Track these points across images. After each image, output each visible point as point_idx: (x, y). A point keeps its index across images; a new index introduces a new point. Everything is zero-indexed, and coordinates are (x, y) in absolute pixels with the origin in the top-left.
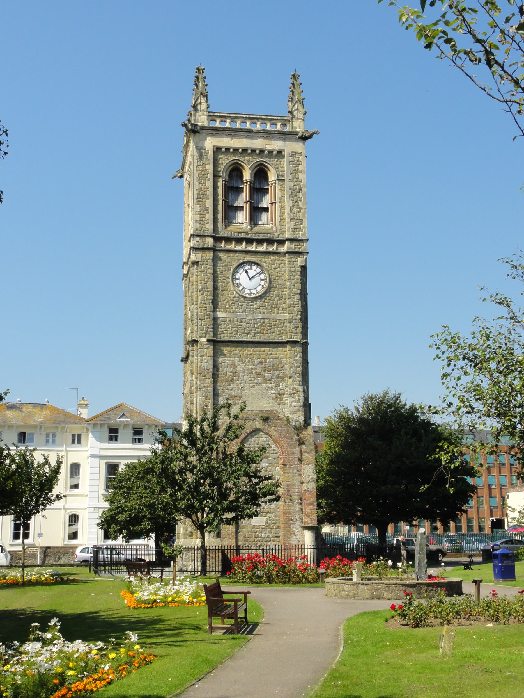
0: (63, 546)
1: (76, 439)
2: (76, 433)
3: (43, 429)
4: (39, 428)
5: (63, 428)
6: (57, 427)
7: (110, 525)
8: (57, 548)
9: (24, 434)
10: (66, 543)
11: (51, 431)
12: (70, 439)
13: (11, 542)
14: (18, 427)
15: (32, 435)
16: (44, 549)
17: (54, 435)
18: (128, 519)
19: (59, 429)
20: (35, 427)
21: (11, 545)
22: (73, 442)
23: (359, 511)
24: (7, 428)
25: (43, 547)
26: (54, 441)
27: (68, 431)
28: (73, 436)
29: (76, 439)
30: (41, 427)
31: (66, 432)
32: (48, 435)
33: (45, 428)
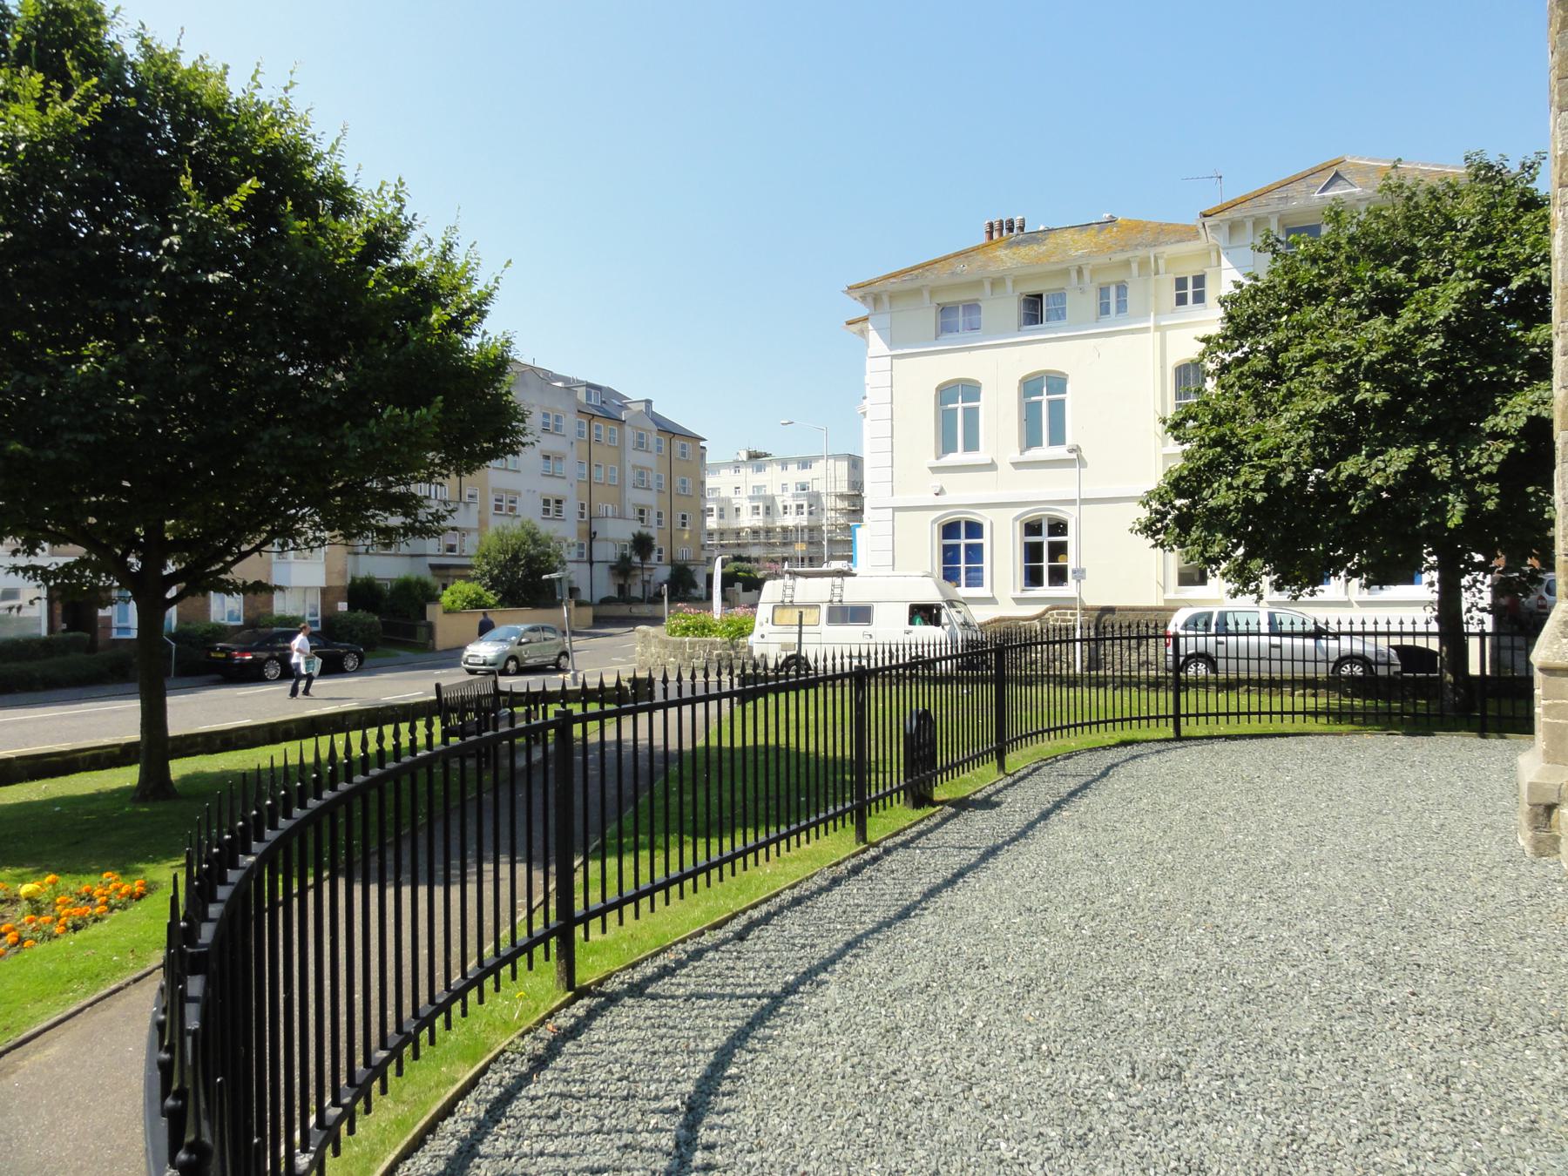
0: (1161, 604)
1: (1190, 291)
2: (1189, 273)
3: (1086, 273)
4: (1074, 274)
5: (1144, 264)
6: (1127, 263)
7: (1187, 516)
8: (1133, 609)
9: (1040, 296)
10: (1171, 595)
11: (1113, 277)
12: (1171, 293)
13: (1018, 594)
14: (1016, 281)
15: (1061, 296)
16: (1096, 614)
17: (1122, 288)
18: (1259, 498)
19: (1134, 266)
20: (1065, 272)
21: (1019, 601)
22: (1181, 300)
23: (144, 345)
24: (987, 286)
25: (1093, 609)
26: (1122, 306)
27: (1162, 270)
28: (1181, 283)
29: (1190, 291)
30: (1080, 271)
31: (1157, 273)
32: (1104, 291)
33: (1014, 282)
